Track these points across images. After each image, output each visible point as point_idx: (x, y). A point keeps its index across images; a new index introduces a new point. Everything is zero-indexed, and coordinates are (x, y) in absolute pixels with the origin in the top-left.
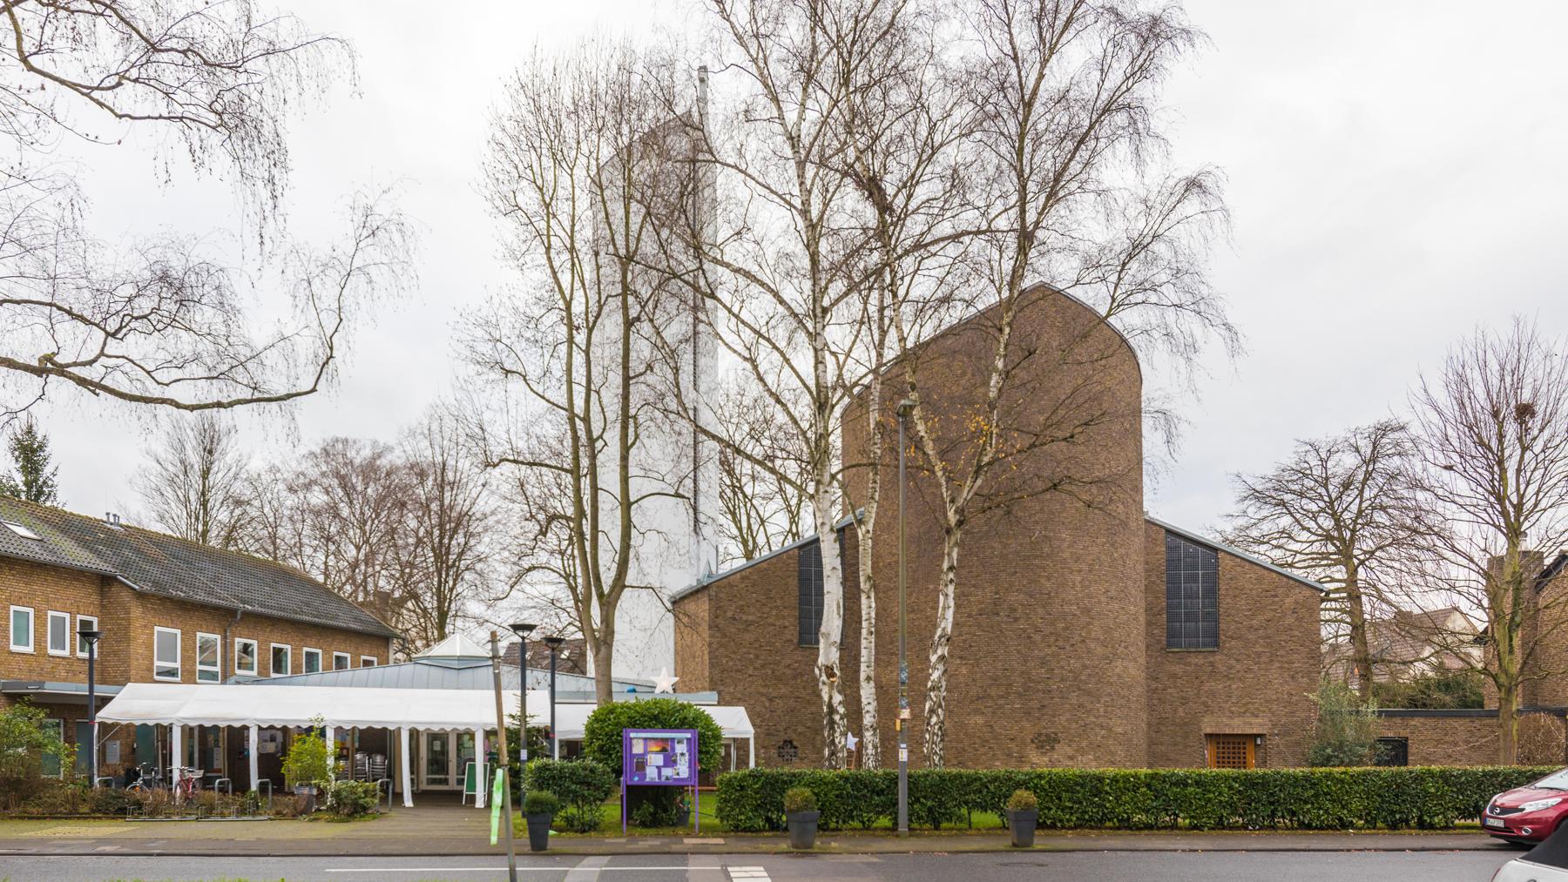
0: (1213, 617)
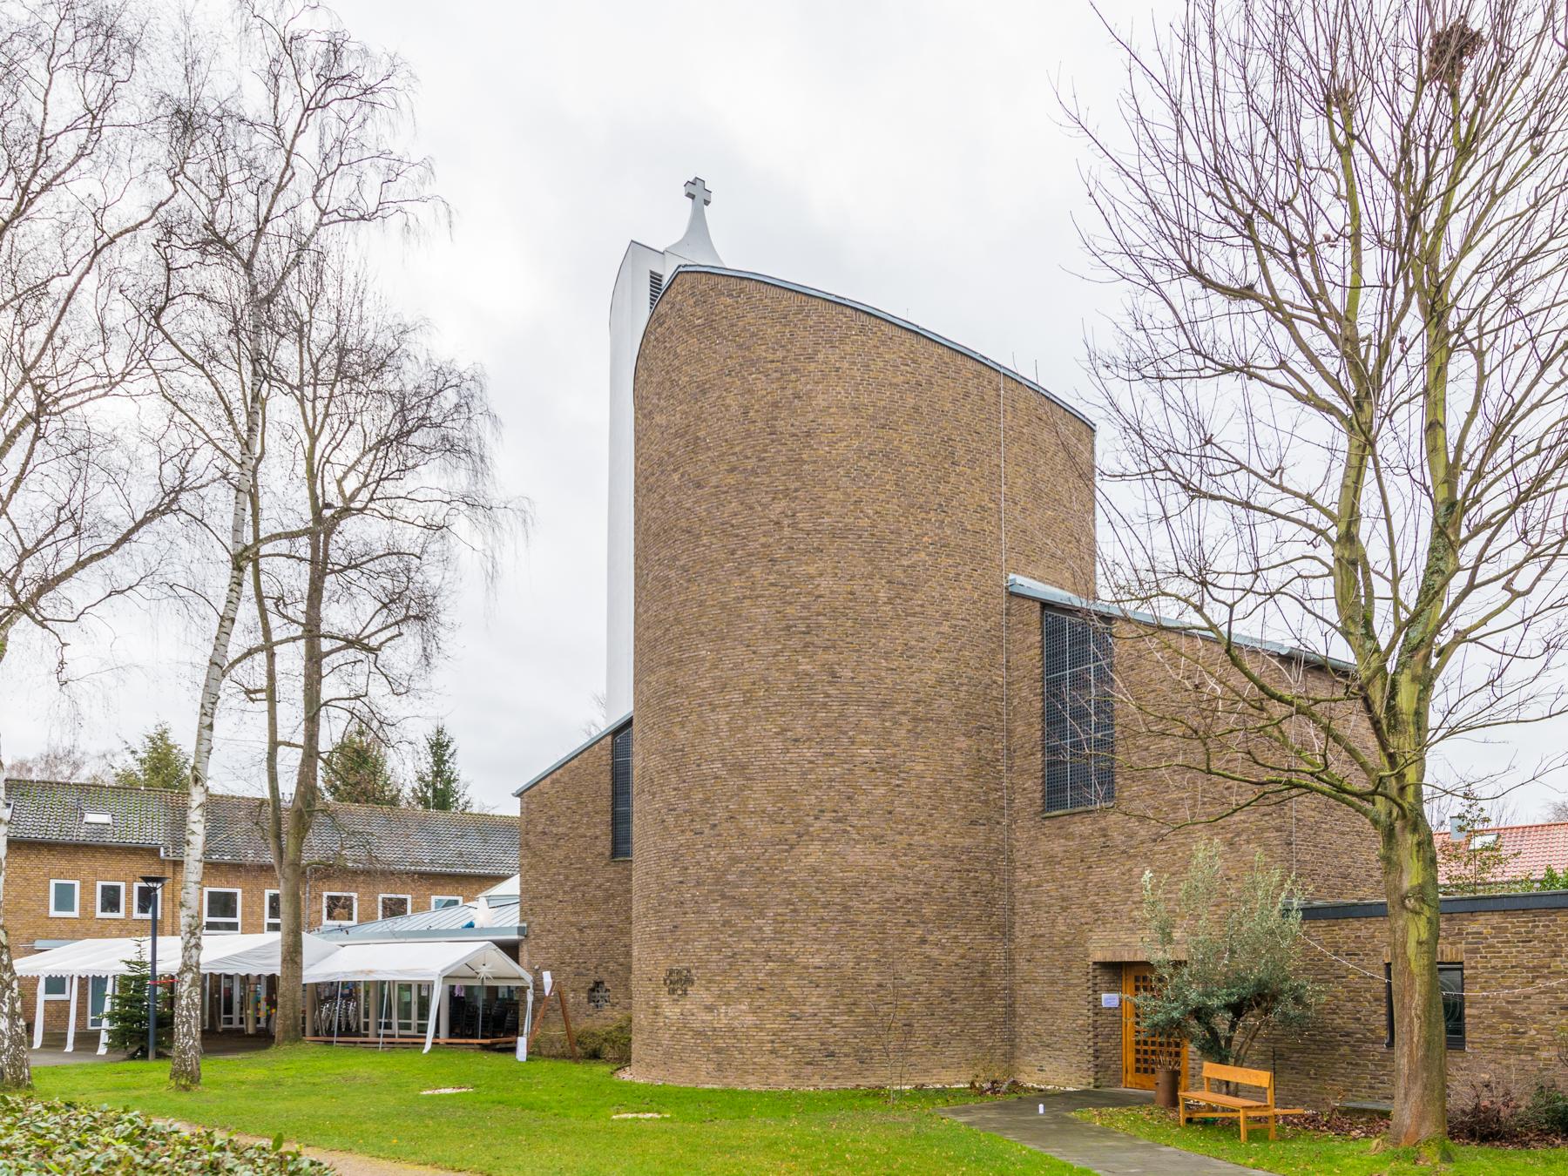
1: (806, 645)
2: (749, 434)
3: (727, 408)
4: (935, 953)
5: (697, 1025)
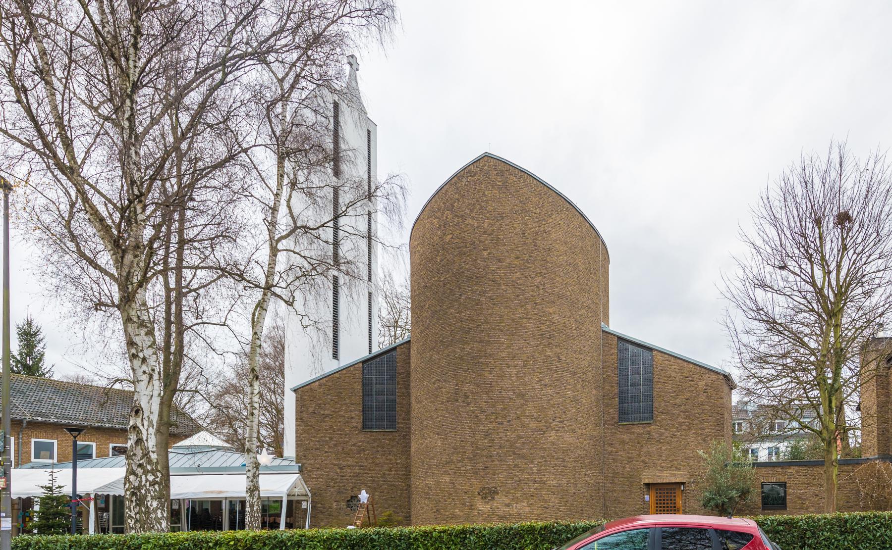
0: (650, 397)
1: (550, 344)
2: (525, 244)
3: (515, 229)
4: (588, 480)
5: (501, 513)
